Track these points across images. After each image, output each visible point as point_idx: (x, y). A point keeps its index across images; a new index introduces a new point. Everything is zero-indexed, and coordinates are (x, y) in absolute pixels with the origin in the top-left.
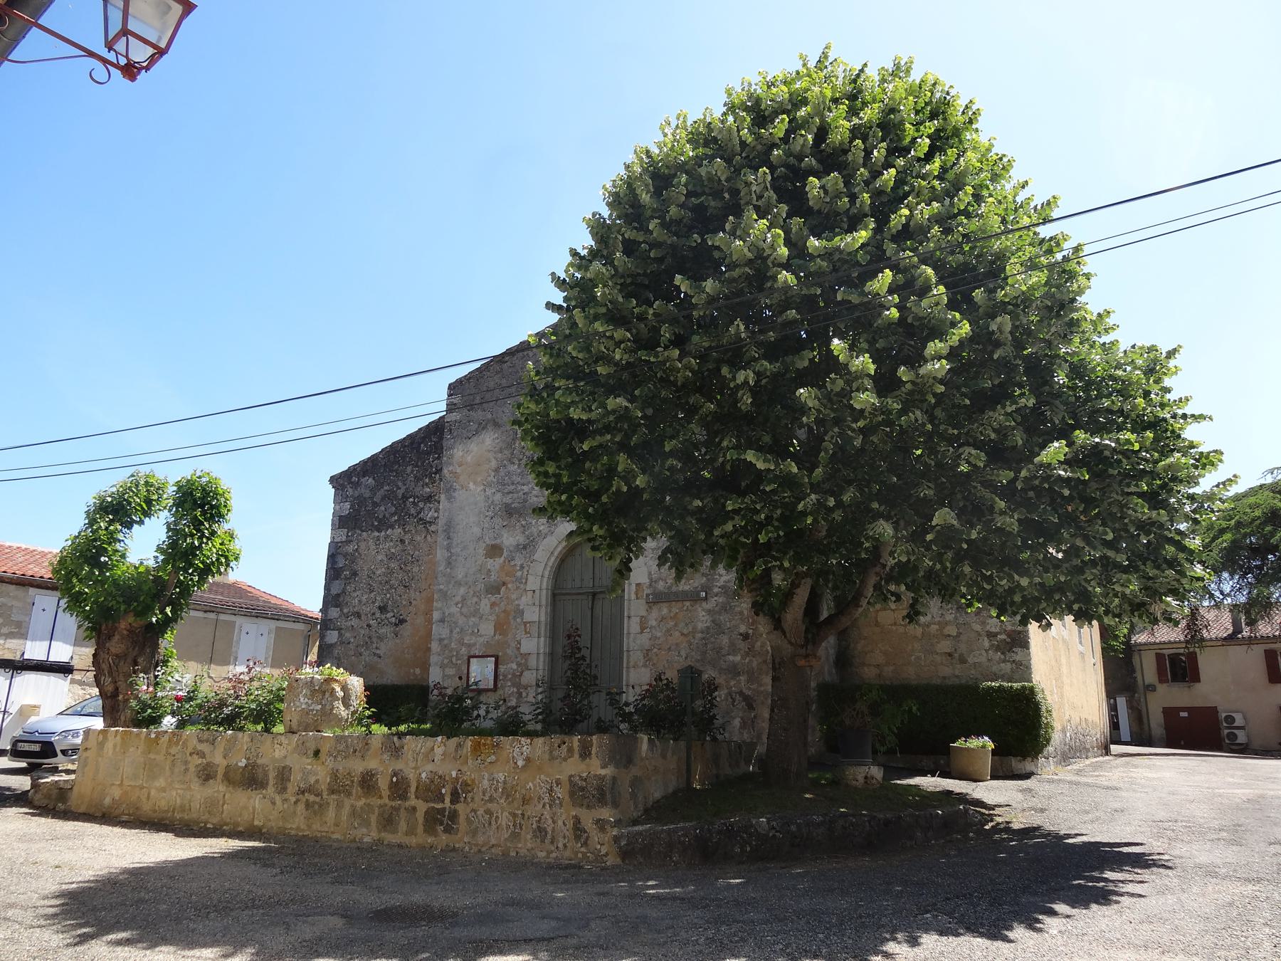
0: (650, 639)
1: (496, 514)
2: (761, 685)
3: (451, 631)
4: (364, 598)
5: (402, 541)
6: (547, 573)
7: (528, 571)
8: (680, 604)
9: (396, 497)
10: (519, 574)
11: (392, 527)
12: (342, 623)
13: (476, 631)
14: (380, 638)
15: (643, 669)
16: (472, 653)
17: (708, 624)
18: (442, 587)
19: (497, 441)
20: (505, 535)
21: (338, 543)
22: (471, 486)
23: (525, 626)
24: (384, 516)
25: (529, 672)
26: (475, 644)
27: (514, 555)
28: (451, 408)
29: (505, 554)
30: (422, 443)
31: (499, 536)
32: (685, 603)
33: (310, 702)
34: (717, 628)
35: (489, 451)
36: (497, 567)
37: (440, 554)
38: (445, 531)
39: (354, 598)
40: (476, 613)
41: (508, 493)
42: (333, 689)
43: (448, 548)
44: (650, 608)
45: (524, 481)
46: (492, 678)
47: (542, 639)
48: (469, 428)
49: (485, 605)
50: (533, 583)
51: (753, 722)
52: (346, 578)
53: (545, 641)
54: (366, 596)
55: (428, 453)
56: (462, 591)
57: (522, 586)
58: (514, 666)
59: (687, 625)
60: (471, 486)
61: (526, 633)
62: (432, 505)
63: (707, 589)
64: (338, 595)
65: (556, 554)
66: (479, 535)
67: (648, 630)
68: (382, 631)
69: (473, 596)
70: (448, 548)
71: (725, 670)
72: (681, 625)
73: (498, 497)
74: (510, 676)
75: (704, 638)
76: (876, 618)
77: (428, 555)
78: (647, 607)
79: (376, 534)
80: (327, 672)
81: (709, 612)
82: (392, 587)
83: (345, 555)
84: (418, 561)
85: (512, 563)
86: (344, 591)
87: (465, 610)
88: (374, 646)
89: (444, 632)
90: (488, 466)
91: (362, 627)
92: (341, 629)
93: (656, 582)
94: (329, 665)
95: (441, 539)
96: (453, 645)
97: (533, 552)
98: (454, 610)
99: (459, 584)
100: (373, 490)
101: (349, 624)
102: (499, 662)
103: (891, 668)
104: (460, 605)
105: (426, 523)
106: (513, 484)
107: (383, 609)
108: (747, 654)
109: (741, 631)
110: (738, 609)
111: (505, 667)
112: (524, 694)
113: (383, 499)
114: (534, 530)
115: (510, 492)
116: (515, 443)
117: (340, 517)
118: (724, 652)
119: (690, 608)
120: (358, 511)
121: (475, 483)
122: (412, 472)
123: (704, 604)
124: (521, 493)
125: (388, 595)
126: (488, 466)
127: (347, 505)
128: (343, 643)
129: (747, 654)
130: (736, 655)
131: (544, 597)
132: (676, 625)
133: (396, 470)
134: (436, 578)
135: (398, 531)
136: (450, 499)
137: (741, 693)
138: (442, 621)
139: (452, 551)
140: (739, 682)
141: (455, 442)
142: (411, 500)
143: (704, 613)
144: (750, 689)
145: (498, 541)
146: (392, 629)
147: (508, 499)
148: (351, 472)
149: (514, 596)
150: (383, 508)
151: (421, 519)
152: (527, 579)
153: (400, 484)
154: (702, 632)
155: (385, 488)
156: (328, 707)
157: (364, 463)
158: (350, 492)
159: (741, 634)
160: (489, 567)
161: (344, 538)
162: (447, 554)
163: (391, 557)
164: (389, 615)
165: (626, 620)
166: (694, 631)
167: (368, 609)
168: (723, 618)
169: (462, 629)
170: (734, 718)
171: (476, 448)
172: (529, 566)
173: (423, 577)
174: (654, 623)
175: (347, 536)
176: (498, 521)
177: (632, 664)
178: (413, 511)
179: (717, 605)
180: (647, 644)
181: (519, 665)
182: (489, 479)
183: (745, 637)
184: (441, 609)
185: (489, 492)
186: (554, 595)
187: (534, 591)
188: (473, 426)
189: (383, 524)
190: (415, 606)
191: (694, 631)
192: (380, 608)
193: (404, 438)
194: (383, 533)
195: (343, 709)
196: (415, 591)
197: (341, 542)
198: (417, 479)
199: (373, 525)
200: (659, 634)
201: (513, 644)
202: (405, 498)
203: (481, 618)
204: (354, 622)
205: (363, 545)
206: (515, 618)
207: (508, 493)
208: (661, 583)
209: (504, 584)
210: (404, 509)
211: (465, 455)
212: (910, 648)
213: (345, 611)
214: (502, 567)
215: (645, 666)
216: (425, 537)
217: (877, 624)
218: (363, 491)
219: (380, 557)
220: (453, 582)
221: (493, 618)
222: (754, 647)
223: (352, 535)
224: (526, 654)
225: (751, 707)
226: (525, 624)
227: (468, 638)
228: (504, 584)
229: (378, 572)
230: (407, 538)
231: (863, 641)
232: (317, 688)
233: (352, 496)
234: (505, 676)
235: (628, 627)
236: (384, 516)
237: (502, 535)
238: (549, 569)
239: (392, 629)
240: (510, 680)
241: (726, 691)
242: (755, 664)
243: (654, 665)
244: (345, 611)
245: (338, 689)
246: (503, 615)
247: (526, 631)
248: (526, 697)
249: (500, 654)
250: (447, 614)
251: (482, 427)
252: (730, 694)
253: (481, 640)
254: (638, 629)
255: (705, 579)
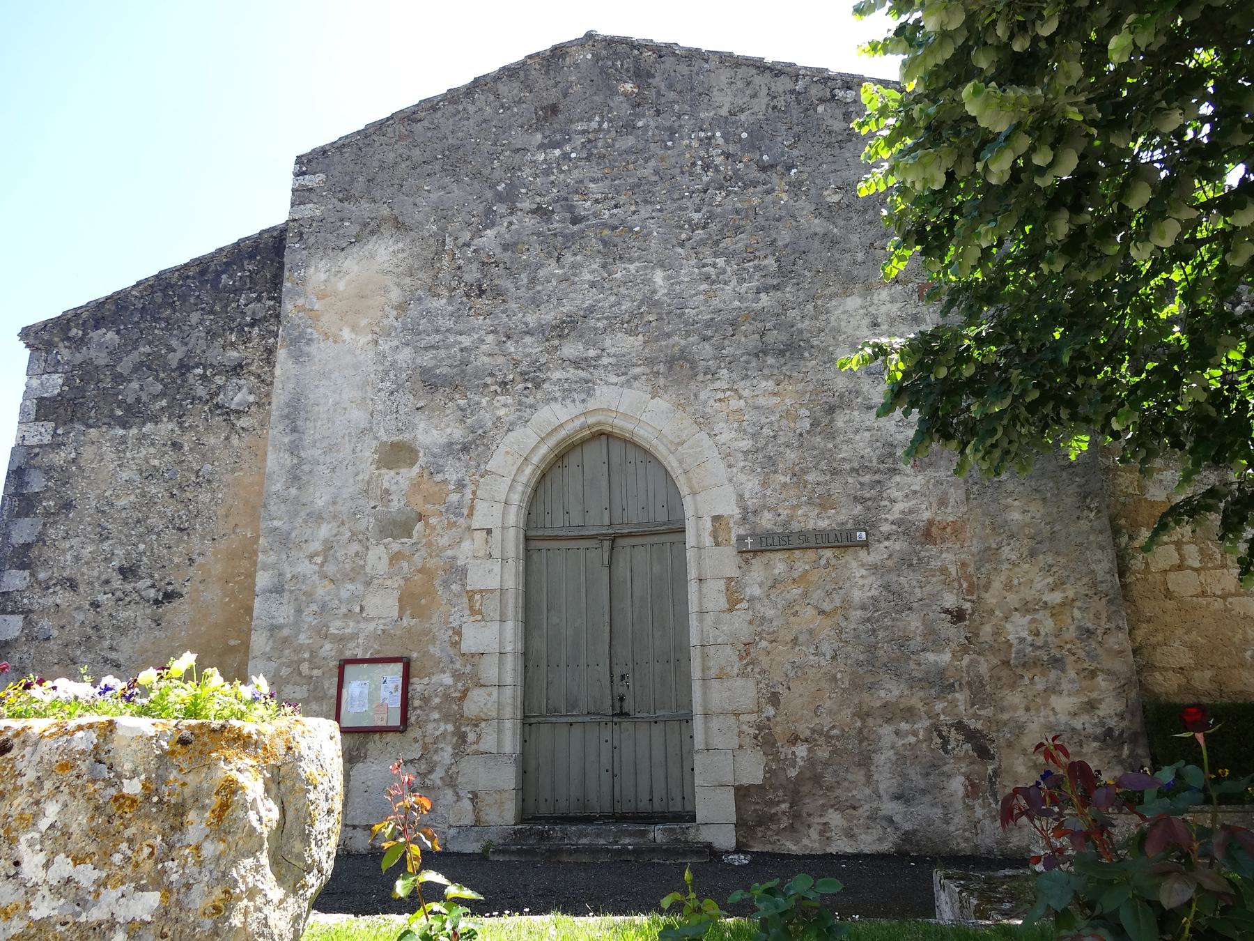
0: (751, 622)
1: (400, 386)
2: (1002, 710)
3: (299, 611)
4: (86, 552)
5: (176, 446)
6: (516, 497)
7: (474, 493)
8: (811, 555)
9: (165, 366)
10: (454, 498)
11: (155, 419)
12: (38, 601)
13: (357, 609)
14: (121, 629)
15: (739, 682)
16: (348, 654)
17: (874, 593)
18: (277, 523)
19: (400, 256)
20: (422, 425)
21: (32, 447)
22: (346, 334)
23: (471, 599)
24: (138, 400)
25: (482, 690)
26: (354, 636)
27: (441, 461)
28: (301, 195)
29: (422, 460)
30: (223, 272)
31: (410, 426)
32: (822, 552)
33: (87, 875)
34: (898, 601)
35: (385, 273)
36: (404, 484)
37: (275, 461)
38: (287, 417)
39: (64, 552)
40: (357, 573)
41: (426, 349)
42: (231, 788)
43: (294, 449)
44: (747, 561)
45: (460, 327)
46: (397, 703)
47: (510, 625)
48: (341, 231)
49: (377, 558)
50: (486, 515)
51: (992, 784)
52: (47, 514)
53: (516, 629)
54: (90, 548)
55: (237, 291)
56: (325, 531)
57: (461, 521)
58: (447, 679)
59: (829, 594)
60: (346, 334)
61: (473, 612)
62: (242, 382)
63: (868, 525)
64: (27, 546)
65: (535, 459)
66: (363, 424)
67: (744, 605)
68: (125, 614)
69: (351, 540)
70: (294, 449)
71: (920, 680)
72: (818, 595)
73: (405, 355)
74: (437, 700)
75: (868, 620)
76: (1165, 582)
77: (233, 471)
78: (738, 559)
79: (120, 432)
80: (182, 694)
81: (874, 568)
82: (150, 530)
83: (48, 471)
84: (209, 481)
85: (439, 478)
86: (41, 539)
87: (331, 569)
88: (107, 644)
89: (284, 612)
90: (383, 300)
91: (79, 608)
92: (31, 611)
93: (755, 512)
94: (188, 660)
95: (277, 433)
96: (303, 639)
97: (487, 453)
98: (305, 567)
99: (317, 517)
100: (116, 354)
101: (50, 601)
102: (412, 670)
103: (1208, 674)
104: (319, 560)
105: (228, 413)
106: (437, 331)
107: (127, 572)
108: (965, 650)
109: (948, 605)
110: (936, 564)
111: (426, 680)
112: (471, 737)
113: (137, 368)
114: (487, 417)
115: (432, 347)
116: (440, 260)
117: (41, 401)
118: (914, 645)
119: (833, 562)
120: (82, 390)
121: (354, 328)
122: (201, 322)
123: (863, 554)
124: (456, 349)
125: (142, 547)
126: (383, 300)
127: (57, 379)
128: (31, 638)
129: (965, 650)
130: (942, 651)
131: (512, 542)
132: (805, 595)
133: (167, 320)
134: (265, 506)
135: (167, 427)
136: (298, 357)
137: (960, 726)
138: (278, 590)
139: (302, 454)
140: (954, 703)
141: (310, 255)
142: (199, 371)
143: (864, 572)
144: (977, 717)
145: (406, 437)
146: (148, 611)
147: (427, 360)
148: (69, 321)
149: (443, 541)
150: (135, 385)
151: (217, 406)
152: (472, 508)
153: (174, 343)
154: (864, 608)
155: (142, 349)
156: (199, 900)
157: (100, 304)
158: (64, 354)
159: (947, 611)
160: (386, 485)
161: (47, 439)
162: (288, 461)
163: (150, 475)
164: (141, 584)
165: (693, 587)
166: (846, 606)
167: (95, 573)
168: (906, 580)
169: (324, 607)
170: (949, 777)
171: (355, 269)
172: (477, 484)
173: (221, 511)
174: (757, 591)
175: (55, 435)
176: (406, 400)
177: (713, 672)
178: (201, 391)
179: (890, 556)
180: (745, 633)
181: (457, 676)
182: (385, 322)
183: (958, 616)
184: (273, 566)
185: (384, 346)
186: (527, 539)
187: (489, 531)
188: (351, 228)
189: (134, 414)
190: (202, 566)
191: (846, 606)
192: (122, 570)
193: (186, 265)
194: (134, 431)
195: (276, 893)
196: (203, 537)
197: (40, 446)
198: (212, 335)
199: (112, 416)
200: (770, 613)
201: (444, 636)
202: (184, 367)
203: (368, 584)
204: (62, 597)
205: (88, 452)
206: (446, 584)
207: (426, 349)
208: (767, 515)
209: (420, 517)
210: (182, 386)
211: (333, 279)
212: (1239, 636)
213: (42, 576)
214: (416, 486)
215: (743, 674)
216: (227, 438)
217: (1168, 595)
218: (93, 353)
219: (125, 475)
220: (303, 514)
221: (397, 582)
222: (977, 635)
223: (66, 434)
224: (473, 655)
225: (984, 753)
226: (471, 594)
227: (338, 623)
228: (420, 517)
229: (123, 502)
230: (187, 441)
231: (1145, 625)
232: (133, 787)
233: (67, 363)
234: (426, 700)
235: (701, 597)
236: (138, 400)
237: (415, 427)
238: (520, 488)
239: (148, 611)
240: (438, 707)
241: (928, 723)
242: (984, 668)
243: (761, 672)
244: (42, 576)
245: (253, 785)
246: (418, 577)
247: (471, 608)
248: (476, 743)
249: (415, 655)
250: (289, 576)
251: (369, 230)
252: (936, 728)
253: (371, 627)
254: (723, 603)
255: (859, 507)
